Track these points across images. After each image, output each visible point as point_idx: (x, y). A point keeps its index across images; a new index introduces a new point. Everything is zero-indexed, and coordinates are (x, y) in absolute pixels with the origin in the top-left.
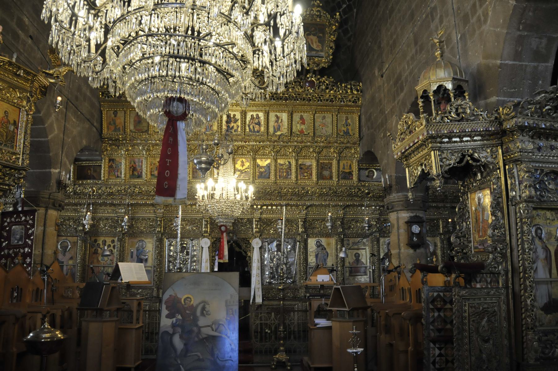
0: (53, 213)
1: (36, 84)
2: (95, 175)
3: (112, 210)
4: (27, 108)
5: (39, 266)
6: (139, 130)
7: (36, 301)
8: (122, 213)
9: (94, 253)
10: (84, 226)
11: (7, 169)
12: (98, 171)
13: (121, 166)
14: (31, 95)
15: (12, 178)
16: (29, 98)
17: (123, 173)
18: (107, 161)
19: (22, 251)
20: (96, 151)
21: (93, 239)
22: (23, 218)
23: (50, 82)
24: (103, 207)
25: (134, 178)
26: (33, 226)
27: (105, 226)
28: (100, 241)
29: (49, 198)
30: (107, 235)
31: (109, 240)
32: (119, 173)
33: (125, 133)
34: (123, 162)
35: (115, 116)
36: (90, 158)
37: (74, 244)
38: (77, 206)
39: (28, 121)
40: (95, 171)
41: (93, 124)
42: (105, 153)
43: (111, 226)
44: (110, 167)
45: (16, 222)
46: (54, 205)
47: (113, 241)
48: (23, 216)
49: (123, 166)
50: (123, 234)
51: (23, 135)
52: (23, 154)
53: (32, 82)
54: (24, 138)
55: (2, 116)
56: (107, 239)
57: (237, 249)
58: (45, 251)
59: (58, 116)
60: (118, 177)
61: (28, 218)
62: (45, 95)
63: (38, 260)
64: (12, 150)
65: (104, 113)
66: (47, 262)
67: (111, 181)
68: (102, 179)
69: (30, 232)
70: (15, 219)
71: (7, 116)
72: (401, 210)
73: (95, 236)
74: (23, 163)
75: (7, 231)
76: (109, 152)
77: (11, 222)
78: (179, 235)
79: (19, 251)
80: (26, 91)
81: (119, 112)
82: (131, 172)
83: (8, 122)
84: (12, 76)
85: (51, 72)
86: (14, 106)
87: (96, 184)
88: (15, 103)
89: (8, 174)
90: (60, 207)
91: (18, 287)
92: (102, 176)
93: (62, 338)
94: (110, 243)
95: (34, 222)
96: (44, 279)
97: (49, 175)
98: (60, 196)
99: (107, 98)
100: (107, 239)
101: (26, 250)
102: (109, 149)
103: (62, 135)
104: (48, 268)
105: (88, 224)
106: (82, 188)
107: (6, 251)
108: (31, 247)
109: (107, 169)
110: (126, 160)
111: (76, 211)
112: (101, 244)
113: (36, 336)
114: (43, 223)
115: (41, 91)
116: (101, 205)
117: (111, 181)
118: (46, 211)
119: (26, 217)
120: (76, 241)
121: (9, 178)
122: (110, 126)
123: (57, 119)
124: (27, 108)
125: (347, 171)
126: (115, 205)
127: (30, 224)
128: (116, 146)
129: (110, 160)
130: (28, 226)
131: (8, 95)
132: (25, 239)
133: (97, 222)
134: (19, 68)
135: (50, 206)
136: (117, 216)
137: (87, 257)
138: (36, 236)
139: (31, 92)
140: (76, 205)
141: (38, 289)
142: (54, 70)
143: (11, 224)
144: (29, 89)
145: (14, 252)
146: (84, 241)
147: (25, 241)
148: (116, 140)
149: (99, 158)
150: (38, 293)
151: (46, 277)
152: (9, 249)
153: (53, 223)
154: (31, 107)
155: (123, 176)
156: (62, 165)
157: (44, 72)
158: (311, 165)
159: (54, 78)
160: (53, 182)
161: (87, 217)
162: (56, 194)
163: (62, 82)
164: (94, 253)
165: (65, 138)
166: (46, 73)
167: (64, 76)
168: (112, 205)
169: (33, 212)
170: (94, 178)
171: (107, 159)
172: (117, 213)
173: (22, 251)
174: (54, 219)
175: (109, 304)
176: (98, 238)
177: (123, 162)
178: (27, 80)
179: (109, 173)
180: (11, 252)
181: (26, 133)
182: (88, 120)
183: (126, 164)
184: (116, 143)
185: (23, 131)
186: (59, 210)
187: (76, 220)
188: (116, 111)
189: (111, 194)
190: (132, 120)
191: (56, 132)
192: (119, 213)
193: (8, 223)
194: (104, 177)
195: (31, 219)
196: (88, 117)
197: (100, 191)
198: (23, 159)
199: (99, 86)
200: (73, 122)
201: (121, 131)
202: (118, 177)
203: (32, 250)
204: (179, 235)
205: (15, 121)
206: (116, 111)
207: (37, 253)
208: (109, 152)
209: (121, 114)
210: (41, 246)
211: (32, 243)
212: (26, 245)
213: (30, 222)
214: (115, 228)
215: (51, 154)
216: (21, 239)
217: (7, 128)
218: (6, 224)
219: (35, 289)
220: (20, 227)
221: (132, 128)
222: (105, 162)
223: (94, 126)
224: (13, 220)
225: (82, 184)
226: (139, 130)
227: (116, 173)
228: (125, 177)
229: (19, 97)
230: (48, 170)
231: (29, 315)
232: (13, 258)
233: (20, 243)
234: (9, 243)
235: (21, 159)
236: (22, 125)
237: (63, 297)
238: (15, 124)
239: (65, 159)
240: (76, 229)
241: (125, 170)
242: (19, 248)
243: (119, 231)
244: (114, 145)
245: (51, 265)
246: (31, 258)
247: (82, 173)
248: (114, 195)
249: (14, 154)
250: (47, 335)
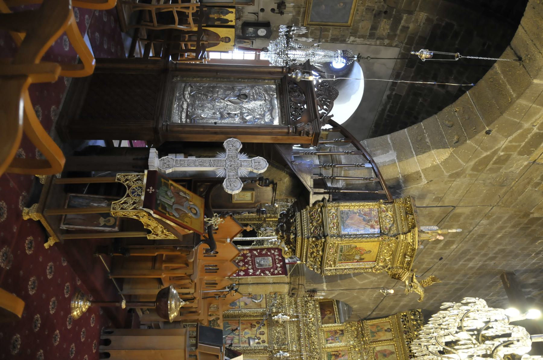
0: (286, 289)
1: (400, 271)
2: (326, 318)
3: (294, 338)
4: (378, 267)
5: (237, 283)
6: (376, 355)
7: (206, 284)
8: (292, 348)
9: (251, 324)
10: (277, 313)
11: (320, 259)
12: (330, 321)
13: (338, 342)
14: (389, 268)
15: (313, 264)
16: (387, 267)
17: (331, 345)
18: (341, 328)
19: (250, 267)
20: (349, 317)
21: (265, 322)
22: (279, 265)
23: (405, 282)
24: (296, 329)
25: (327, 356)
26: (273, 274)
27: (278, 333)
28: (264, 329)
29: (299, 284)
30: (270, 336)
31: (264, 337)
32: (331, 341)
33: (371, 342)
34: (343, 344)
35: (386, 331)
36: (341, 311)
37: (259, 306)
38: (295, 304)
39: (366, 269)
40: (329, 318)
41: (374, 311)
42: (348, 325)
43: (278, 338)
44: (336, 332)
45: (275, 260)
46: (293, 289)
47: (264, 342)
49: (338, 344)
50: (271, 351)
51: (351, 267)
52: (335, 269)
53: (402, 268)
54: (349, 269)
55: (366, 249)
56: (266, 335)
58: (251, 286)
59: (376, 282)
60: (327, 340)
61: (279, 269)
62: (392, 278)
63: (243, 281)
64: (337, 260)
65: (387, 319)
66: (241, 289)
67: (321, 334)
68: (323, 326)
69: (267, 272)
70: (278, 259)
71: (367, 253)
73: (267, 323)
74: (327, 270)
76: (349, 329)
77: (275, 256)
79: (249, 265)
80: (392, 264)
81: (390, 333)
82: (334, 353)
83: (362, 254)
84: (403, 252)
85: (415, 280)
86: (377, 256)
87: (318, 321)
88: (379, 257)
89: (316, 260)
90: (292, 293)
91: (218, 269)
92: (326, 325)
93: (170, 318)
94: (262, 339)
95: (276, 274)
96: (225, 288)
97: (320, 282)
98: (302, 292)
99: (402, 320)
100: (266, 335)
101: (251, 271)
102: (353, 328)
103: (358, 287)
104: (236, 291)
105: (279, 318)
106: (312, 307)
108: (254, 274)
109: (333, 329)
110: (344, 346)
111: (291, 303)
112: (261, 330)
113: (173, 296)
114: (276, 282)
115: (395, 275)
116: (298, 326)
117: (321, 334)
118: (288, 283)
119: (280, 267)
120: (262, 306)
121: (312, 261)
122: (375, 327)
123: (372, 282)
124: (378, 267)
126: (299, 340)
128: (357, 335)
129: (342, 331)
130: (272, 270)
131: (385, 251)
132: (261, 269)
133: (281, 325)
134: (411, 257)
135: (292, 286)
136: (288, 343)
137: (248, 319)
138: (264, 278)
139: (393, 268)
140: (296, 303)
141: (217, 284)
142: (417, 282)
144: (395, 266)
145: (249, 261)
146: (263, 314)
147: (259, 269)
148: (363, 335)
149: (343, 321)
150: (213, 284)
151: (227, 290)
152: (251, 257)
153: (277, 290)
154: (379, 270)
155: (329, 345)
156: (330, 291)
157: (413, 275)
159: (409, 283)
160: (313, 286)
161: (285, 316)
162: (303, 290)
163: (408, 291)
164: (251, 324)
166: (412, 278)
167: (414, 291)
168: (299, 337)
169: (285, 272)
170: (322, 318)
171: (343, 328)
172: (292, 342)
173: (250, 267)
174: (281, 290)
175: (202, 354)
176: (266, 327)
177: (343, 344)
178: (402, 263)
179: (330, 331)
180: (249, 258)
181: (355, 269)
182: (377, 307)
183: (340, 347)
184: (360, 335)
185: (356, 267)
186: (289, 293)
187: (281, 305)
188: (391, 330)
189: (309, 336)
190: (385, 348)
191: (360, 283)
192: (292, 345)
193: (274, 254)
194: (325, 327)
195: (278, 272)
196: (380, 307)
197: (311, 325)
198: (330, 270)
199: (414, 351)
200: (373, 295)
201: (373, 338)
202: (327, 340)
203: (251, 275)
205: (363, 259)
206: (391, 330)
207: (249, 280)
208: (349, 329)
209: (389, 336)
210: (255, 282)
211: (257, 275)
212: (255, 270)
213: (276, 272)
214: (277, 343)
215: (339, 281)
216: (260, 265)
217: (357, 254)
218: (273, 252)
219: (216, 282)
220: (271, 264)
221: (378, 349)
222: (340, 326)
223: (372, 313)
224: (277, 257)
225: (316, 308)
226: (376, 355)
227: (330, 339)
228: (328, 348)
229: (385, 260)
230: (324, 280)
231: (193, 284)
232: (243, 261)
233: (257, 265)
234: (256, 256)
235: (330, 268)
236: (362, 265)
237: (210, 304)
238: (361, 260)
239: (336, 293)
240: (273, 305)
241: (335, 347)
243: (274, 347)
244: (358, 333)
245: (239, 292)
246: (244, 275)
247: (326, 307)
248: (309, 339)
249: (335, 263)
250: (173, 305)
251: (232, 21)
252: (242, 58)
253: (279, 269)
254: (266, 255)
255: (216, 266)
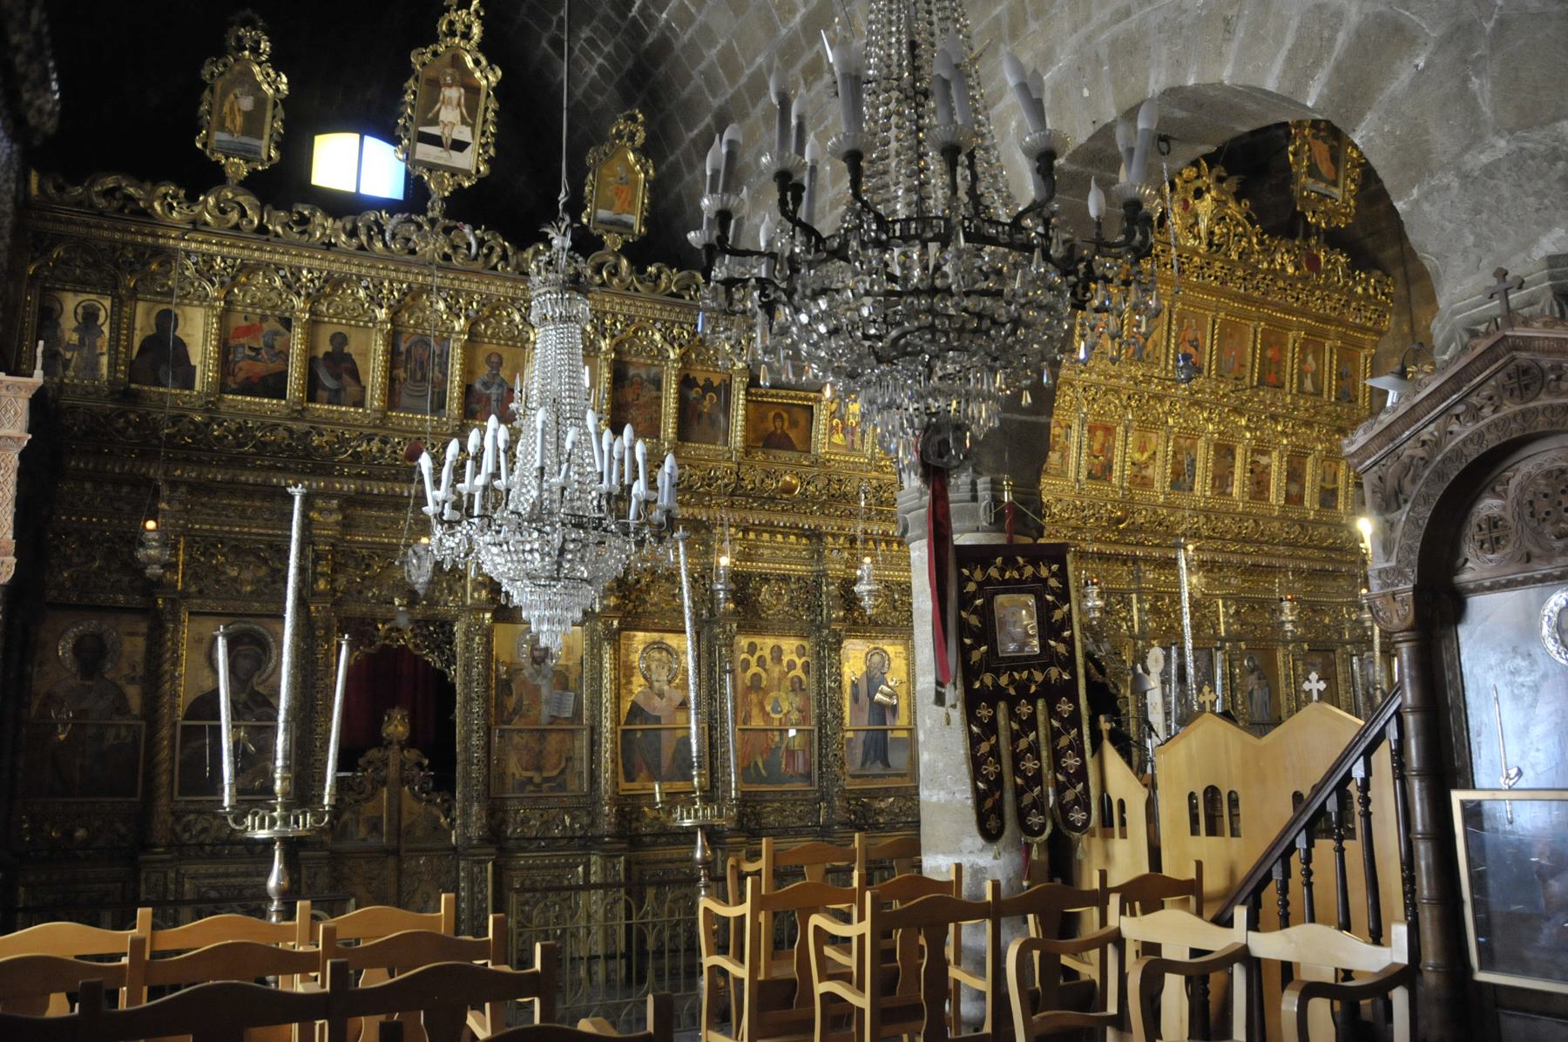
48: (1028, 562)
57: (1099, 678)
72: (1494, 587)
75: (976, 611)
78: (1377, 640)
79: (1030, 679)
107: (988, 679)
119: (1036, 566)
125: (1329, 486)
127: (1053, 591)
143: (990, 589)
145: (1012, 681)
158: (1268, 466)
165: (1404, 293)
180: (1004, 681)
195: (1054, 575)
204: (1377, 640)
213: (1053, 582)
218: (971, 587)
242: (1027, 667)
251: (584, 331)
252: (352, 189)
253: (1044, 572)
254: (987, 613)
255: (1192, 796)
